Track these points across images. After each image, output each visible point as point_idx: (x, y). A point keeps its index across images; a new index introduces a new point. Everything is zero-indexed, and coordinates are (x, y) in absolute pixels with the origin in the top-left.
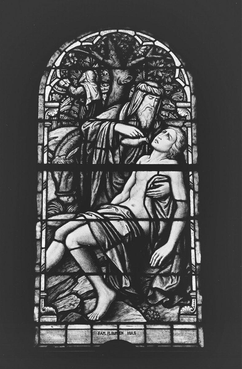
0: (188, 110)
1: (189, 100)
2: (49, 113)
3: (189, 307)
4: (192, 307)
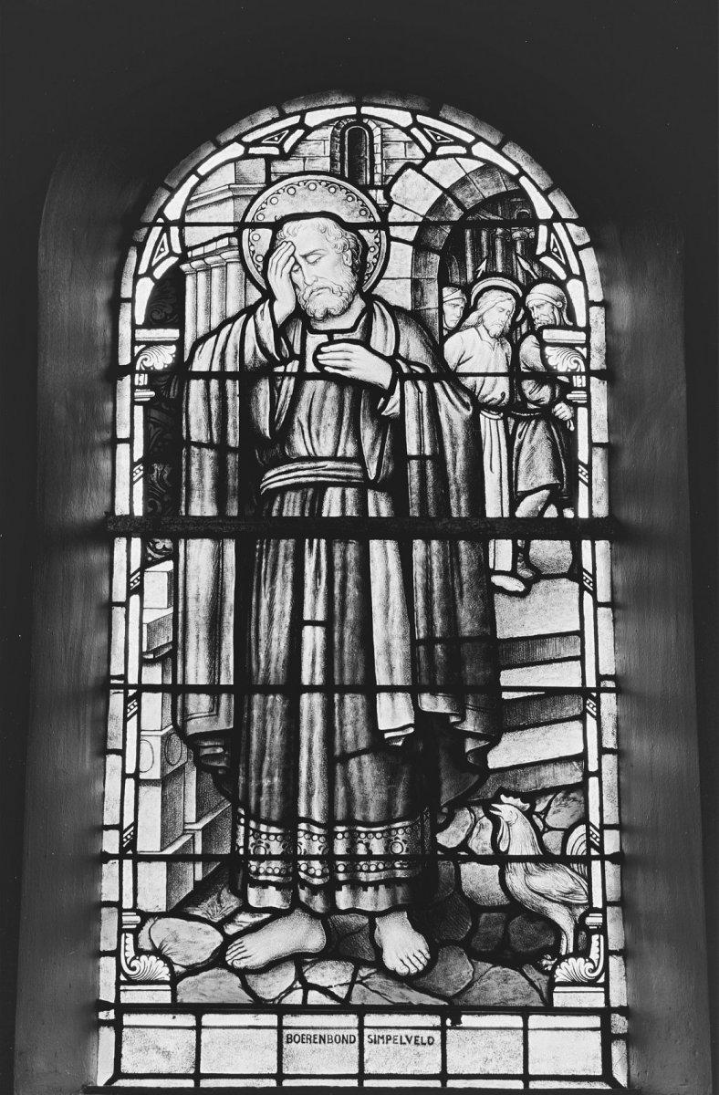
0: (578, 352)
1: (581, 322)
2: (146, 359)
3: (581, 960)
4: (591, 961)
